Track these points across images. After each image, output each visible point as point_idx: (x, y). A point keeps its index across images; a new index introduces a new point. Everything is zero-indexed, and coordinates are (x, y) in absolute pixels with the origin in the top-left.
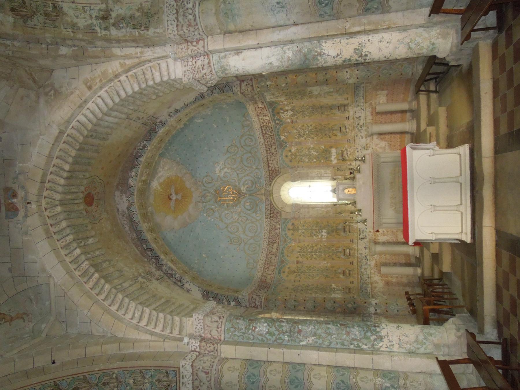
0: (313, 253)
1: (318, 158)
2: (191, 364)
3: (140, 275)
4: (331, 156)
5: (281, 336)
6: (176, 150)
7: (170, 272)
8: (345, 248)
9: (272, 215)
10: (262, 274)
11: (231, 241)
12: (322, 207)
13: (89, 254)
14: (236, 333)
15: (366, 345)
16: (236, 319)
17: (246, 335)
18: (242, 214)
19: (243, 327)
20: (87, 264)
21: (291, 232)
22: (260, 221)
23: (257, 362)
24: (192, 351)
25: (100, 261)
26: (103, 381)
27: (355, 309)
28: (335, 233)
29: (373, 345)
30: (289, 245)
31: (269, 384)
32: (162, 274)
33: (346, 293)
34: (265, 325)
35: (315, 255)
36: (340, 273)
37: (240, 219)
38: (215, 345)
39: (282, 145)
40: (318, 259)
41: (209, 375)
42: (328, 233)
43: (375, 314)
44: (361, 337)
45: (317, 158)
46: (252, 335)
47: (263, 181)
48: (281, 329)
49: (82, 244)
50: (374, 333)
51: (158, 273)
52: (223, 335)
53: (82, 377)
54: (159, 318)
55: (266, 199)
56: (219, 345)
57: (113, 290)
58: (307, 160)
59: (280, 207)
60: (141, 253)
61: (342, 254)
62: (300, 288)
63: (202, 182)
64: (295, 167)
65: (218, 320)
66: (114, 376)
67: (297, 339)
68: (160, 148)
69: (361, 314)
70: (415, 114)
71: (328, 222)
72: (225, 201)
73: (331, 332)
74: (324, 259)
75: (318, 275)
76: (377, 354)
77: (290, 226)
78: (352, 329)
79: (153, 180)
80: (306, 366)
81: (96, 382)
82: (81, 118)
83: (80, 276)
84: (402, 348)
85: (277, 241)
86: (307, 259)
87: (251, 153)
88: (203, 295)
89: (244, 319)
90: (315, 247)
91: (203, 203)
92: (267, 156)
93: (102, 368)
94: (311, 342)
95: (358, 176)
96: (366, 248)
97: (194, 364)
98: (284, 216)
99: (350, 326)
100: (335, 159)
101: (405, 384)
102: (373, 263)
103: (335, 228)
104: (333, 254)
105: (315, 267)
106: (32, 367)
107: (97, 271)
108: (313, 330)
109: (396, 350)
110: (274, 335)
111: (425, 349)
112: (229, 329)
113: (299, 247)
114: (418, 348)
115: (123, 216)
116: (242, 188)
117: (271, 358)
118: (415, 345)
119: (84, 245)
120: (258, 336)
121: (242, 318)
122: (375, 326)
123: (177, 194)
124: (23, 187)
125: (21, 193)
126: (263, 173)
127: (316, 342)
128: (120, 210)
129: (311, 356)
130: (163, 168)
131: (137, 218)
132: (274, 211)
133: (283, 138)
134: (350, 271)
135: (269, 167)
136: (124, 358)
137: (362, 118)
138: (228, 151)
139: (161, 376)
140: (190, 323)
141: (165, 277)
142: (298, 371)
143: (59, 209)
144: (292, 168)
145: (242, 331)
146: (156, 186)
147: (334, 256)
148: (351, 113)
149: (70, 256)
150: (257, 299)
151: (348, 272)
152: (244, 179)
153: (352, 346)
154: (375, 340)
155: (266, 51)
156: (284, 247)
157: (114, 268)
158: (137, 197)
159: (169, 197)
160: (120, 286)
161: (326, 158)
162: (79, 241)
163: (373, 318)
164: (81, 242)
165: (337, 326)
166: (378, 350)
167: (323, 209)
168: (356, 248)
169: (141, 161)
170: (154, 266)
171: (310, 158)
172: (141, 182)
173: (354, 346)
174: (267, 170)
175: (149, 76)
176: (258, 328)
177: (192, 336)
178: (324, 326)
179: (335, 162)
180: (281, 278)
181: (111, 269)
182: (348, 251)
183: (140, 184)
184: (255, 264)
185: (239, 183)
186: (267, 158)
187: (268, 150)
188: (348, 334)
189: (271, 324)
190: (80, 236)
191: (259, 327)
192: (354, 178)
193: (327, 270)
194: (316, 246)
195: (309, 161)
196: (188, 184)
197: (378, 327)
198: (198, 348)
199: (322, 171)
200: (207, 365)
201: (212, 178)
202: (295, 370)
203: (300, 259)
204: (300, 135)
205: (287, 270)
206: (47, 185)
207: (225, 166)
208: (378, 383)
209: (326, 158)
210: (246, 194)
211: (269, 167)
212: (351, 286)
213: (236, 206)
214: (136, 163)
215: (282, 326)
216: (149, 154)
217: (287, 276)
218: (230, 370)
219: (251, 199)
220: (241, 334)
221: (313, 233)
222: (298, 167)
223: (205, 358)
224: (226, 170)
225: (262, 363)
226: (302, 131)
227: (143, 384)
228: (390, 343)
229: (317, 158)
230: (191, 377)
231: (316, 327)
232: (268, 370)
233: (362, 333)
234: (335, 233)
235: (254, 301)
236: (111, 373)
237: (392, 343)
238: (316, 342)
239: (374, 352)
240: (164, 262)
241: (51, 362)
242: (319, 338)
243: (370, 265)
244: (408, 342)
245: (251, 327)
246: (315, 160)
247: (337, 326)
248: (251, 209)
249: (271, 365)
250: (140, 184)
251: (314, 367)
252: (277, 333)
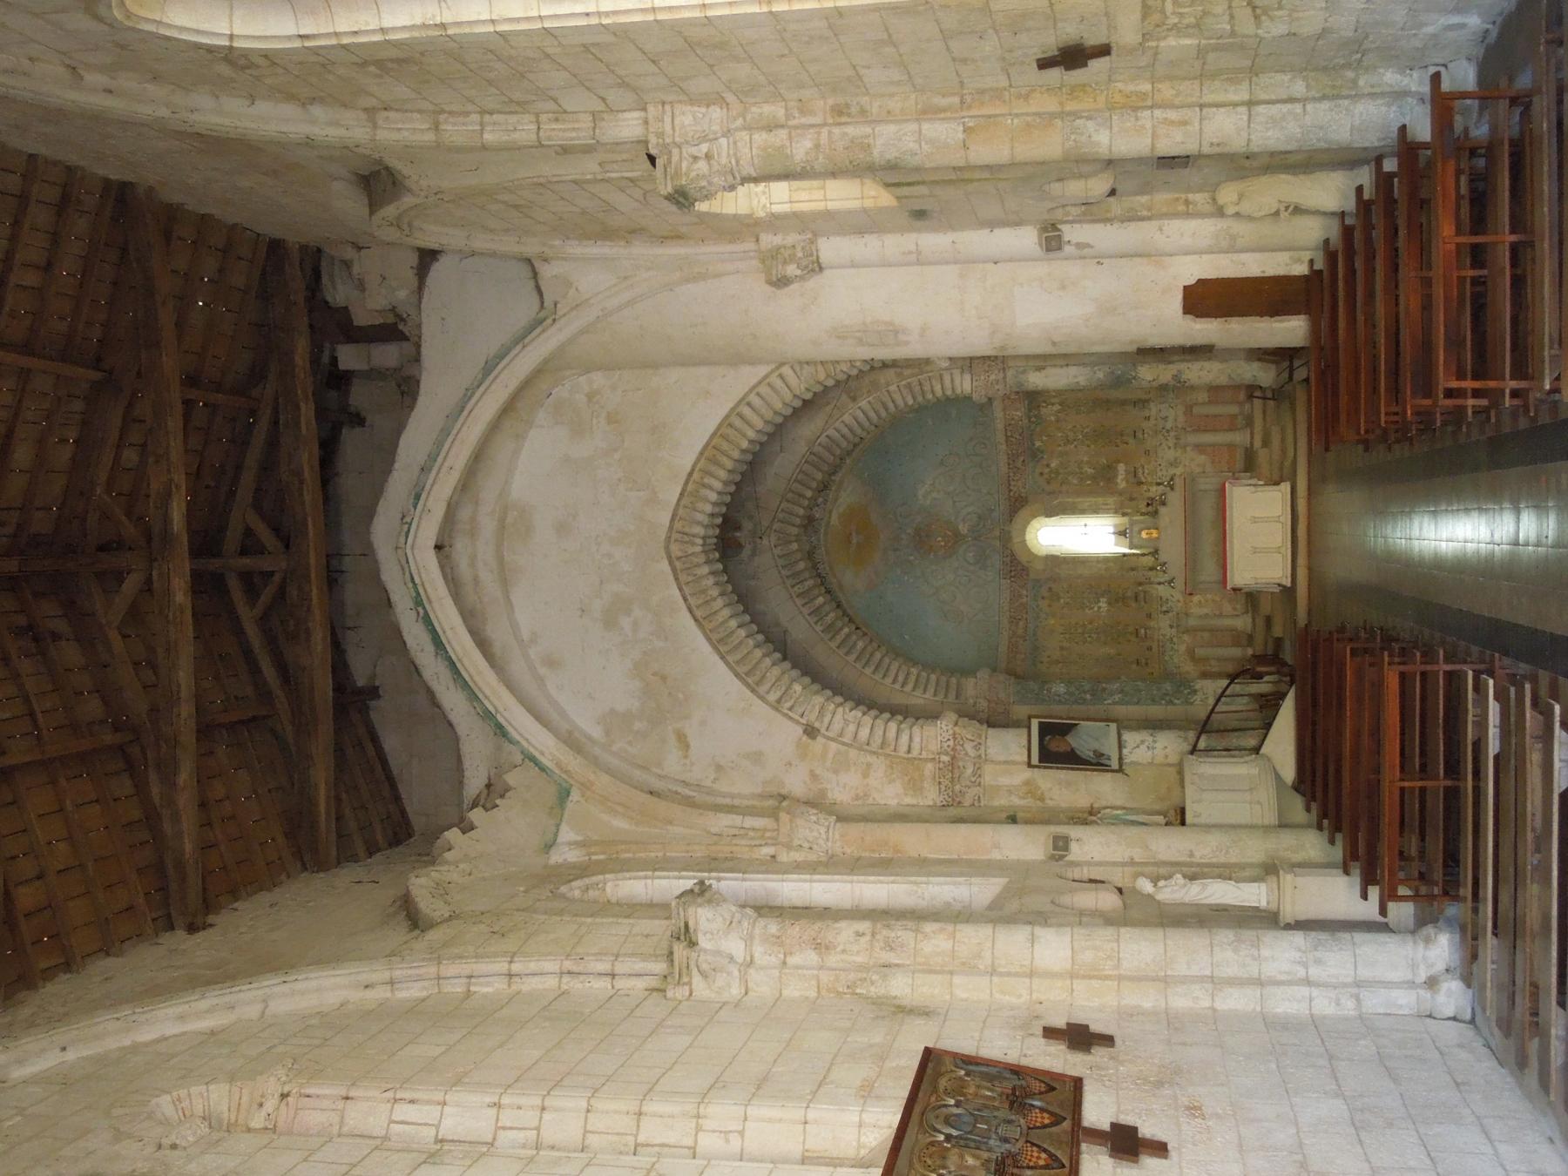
4: (1116, 476)
21: (1047, 602)
39: (1035, 455)
42: (1109, 604)
45: (1093, 478)
70: (1249, 422)
77: (1044, 591)
82: (831, 432)
91: (896, 550)
95: (1163, 510)
98: (1032, 576)
102: (1183, 648)
124: (751, 518)
125: (747, 525)
132: (1022, 570)
133: (1038, 444)
137: (1171, 419)
143: (795, 546)
148: (1154, 411)
155: (1073, 370)
175: (927, 388)
179: (1122, 485)
187: (1012, 458)
192: (1156, 512)
199: (1100, 500)
203: (1065, 644)
204: (1068, 442)
206: (781, 516)
224: (934, 495)
226: (1071, 435)
229: (1093, 478)
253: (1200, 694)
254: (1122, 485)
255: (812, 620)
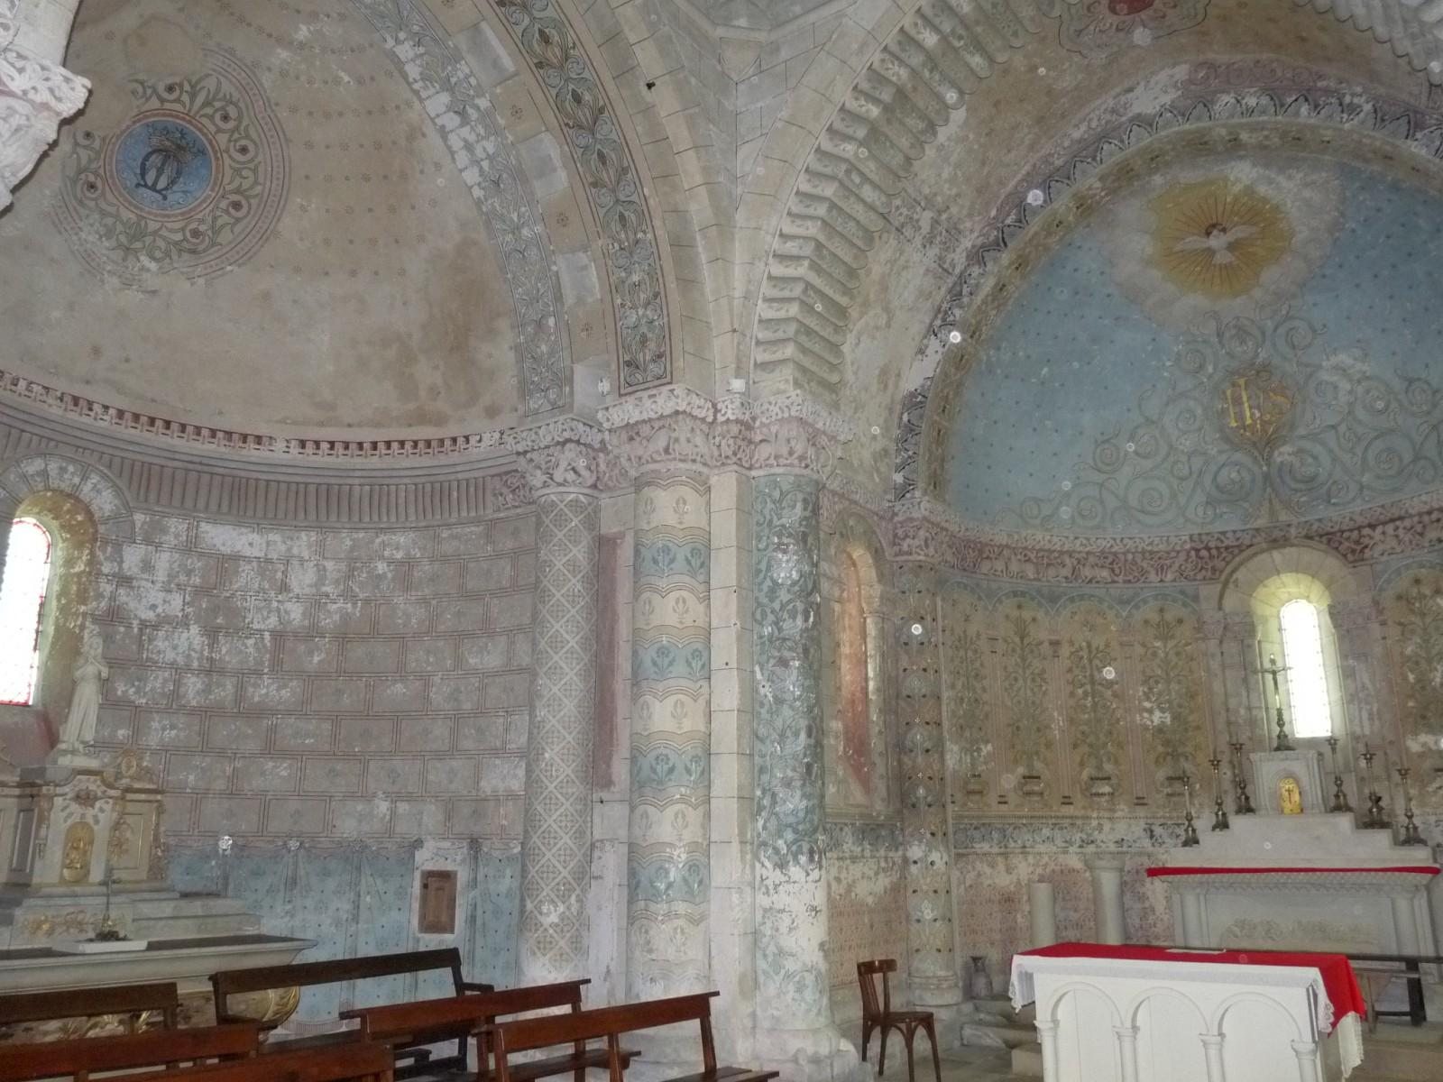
0: (1088, 687)
1: (1423, 688)
2: (680, 409)
3: (940, 212)
5: (771, 618)
6: (1379, 210)
7: (966, 290)
8: (1114, 781)
9: (1204, 553)
10: (1007, 546)
11: (1103, 442)
12: (1249, 709)
13: (931, 71)
14: (770, 505)
15: (765, 828)
16: (805, 501)
17: (767, 531)
18: (1197, 463)
19: (784, 521)
20: (898, 75)
22: (1181, 520)
23: (705, 565)
24: (714, 406)
25: (921, 104)
26: (626, 214)
27: (914, 806)
28: (1160, 749)
29: (765, 844)
30: (1110, 615)
31: (656, 599)
32: (957, 271)
33: (966, 783)
34: (794, 573)
35: (1086, 694)
36: (1030, 766)
37: (1184, 459)
38: (734, 459)
40: (1072, 702)
41: (664, 457)
42: (1160, 730)
43: (905, 860)
44: (782, 816)
46: (767, 546)
47: (1322, 511)
48: (786, 615)
49: (957, 44)
50: (794, 848)
51: (959, 258)
52: (761, 473)
53: (626, 164)
54: (786, 306)
55: (1257, 530)
56: (735, 467)
57: (844, 167)
58: (1409, 651)
59: (1238, 575)
60: (1010, 194)
61: (1094, 773)
62: (970, 654)
63: (1288, 318)
64: (1381, 612)
65: (796, 455)
66: (640, 235)
67: (765, 657)
68: (1366, 161)
69: (902, 821)
71: (1198, 728)
72: (1237, 401)
73: (788, 741)
74: (1072, 721)
75: (1019, 702)
76: (743, 853)
78: (798, 793)
79: (1254, 165)
80: (704, 683)
81: (622, 198)
83: (870, 68)
84: (764, 917)
85: (1120, 579)
86: (1070, 670)
87: (1416, 459)
88: (913, 395)
89: (806, 518)
90: (1110, 692)
91: (1220, 335)
92: (1411, 516)
93: (651, 202)
94: (762, 691)
96: (1120, 842)
97: (681, 417)
99: (808, 789)
100: (1424, 745)
101: (677, 916)
103: (1180, 750)
104: (1091, 746)
105: (1045, 693)
106: (632, 42)
107: (887, 109)
108: (788, 697)
109: (758, 901)
110: (772, 600)
111: (764, 972)
112: (776, 485)
113: (1107, 646)
114: (765, 956)
115: (1113, 111)
116: (1287, 449)
117: (717, 597)
118: (772, 949)
119: (956, 50)
120: (766, 560)
121: (807, 514)
122: (811, 852)
123: (1231, 247)
126: (1346, 511)
127: (762, 705)
128: (1130, 95)
129: (727, 694)
130: (1306, 185)
131: (1111, 154)
132: (1222, 563)
134: (1041, 794)
135: (1372, 526)
136: (681, 244)
138: (1411, 382)
139: (652, 345)
140: (782, 386)
141: (950, 281)
142: (689, 664)
144: (1376, 603)
145: (775, 518)
146: (1238, 180)
147: (1085, 749)
149: (916, 25)
150: (916, 542)
151: (1036, 788)
152: (1318, 449)
153: (759, 793)
154: (776, 851)
156: (1101, 601)
157: (912, 146)
158: (1177, 133)
159: (1214, 226)
160: (857, 180)
161: (1424, 717)
162: (962, 32)
163: (891, 854)
164: (960, 38)
165: (805, 756)
166: (756, 857)
167: (1242, 712)
168: (1119, 814)
169: (1297, 114)
170: (980, 241)
171: (1417, 663)
172: (1230, 134)
173: (761, 799)
174: (1360, 520)
176: (785, 558)
177: (747, 400)
178: (803, 723)
180: (1000, 601)
181: (904, 142)
182: (1107, 789)
183: (1223, 132)
184: (1038, 521)
185: (1303, 437)
186: (1401, 518)
188: (788, 783)
189: (797, 588)
190: (979, 29)
191: (788, 561)
193: (1039, 730)
194: (1115, 695)
195: (1409, 658)
196: (1270, 275)
197: (811, 860)
198: (724, 419)
200: (683, 448)
201: (1310, 345)
202: (690, 657)
203: (1065, 651)
205: (1027, 615)
207: (1359, 382)
208: (676, 853)
209: (1424, 717)
210: (1269, 465)
211: (1372, 526)
212: (992, 799)
213: (1227, 440)
214: (1289, 100)
215: (794, 618)
216: (1329, 132)
217: (1007, 617)
218: (677, 503)
219: (1253, 480)
220: (768, 517)
221: (1157, 682)
222: (1383, 623)
223: (699, 440)
224: (1345, 386)
225: (701, 578)
227: (634, 307)
228: (771, 887)
230: (653, 415)
231: (798, 703)
232: (685, 594)
233: (791, 820)
234: (1160, 749)
235: (911, 534)
236: (644, 227)
237: (772, 891)
238: (762, 705)
239: (749, 847)
240: (990, 266)
241: (649, 79)
242: (770, 711)
243: (1065, 852)
244: (777, 930)
245: (785, 540)
246: (1411, 677)
247: (805, 756)
248: (1217, 487)
249: (699, 598)
250: (1223, 132)
251: (702, 701)
252: (777, 605)
253: (776, 876)
254: (1414, 745)
255: (891, 39)
